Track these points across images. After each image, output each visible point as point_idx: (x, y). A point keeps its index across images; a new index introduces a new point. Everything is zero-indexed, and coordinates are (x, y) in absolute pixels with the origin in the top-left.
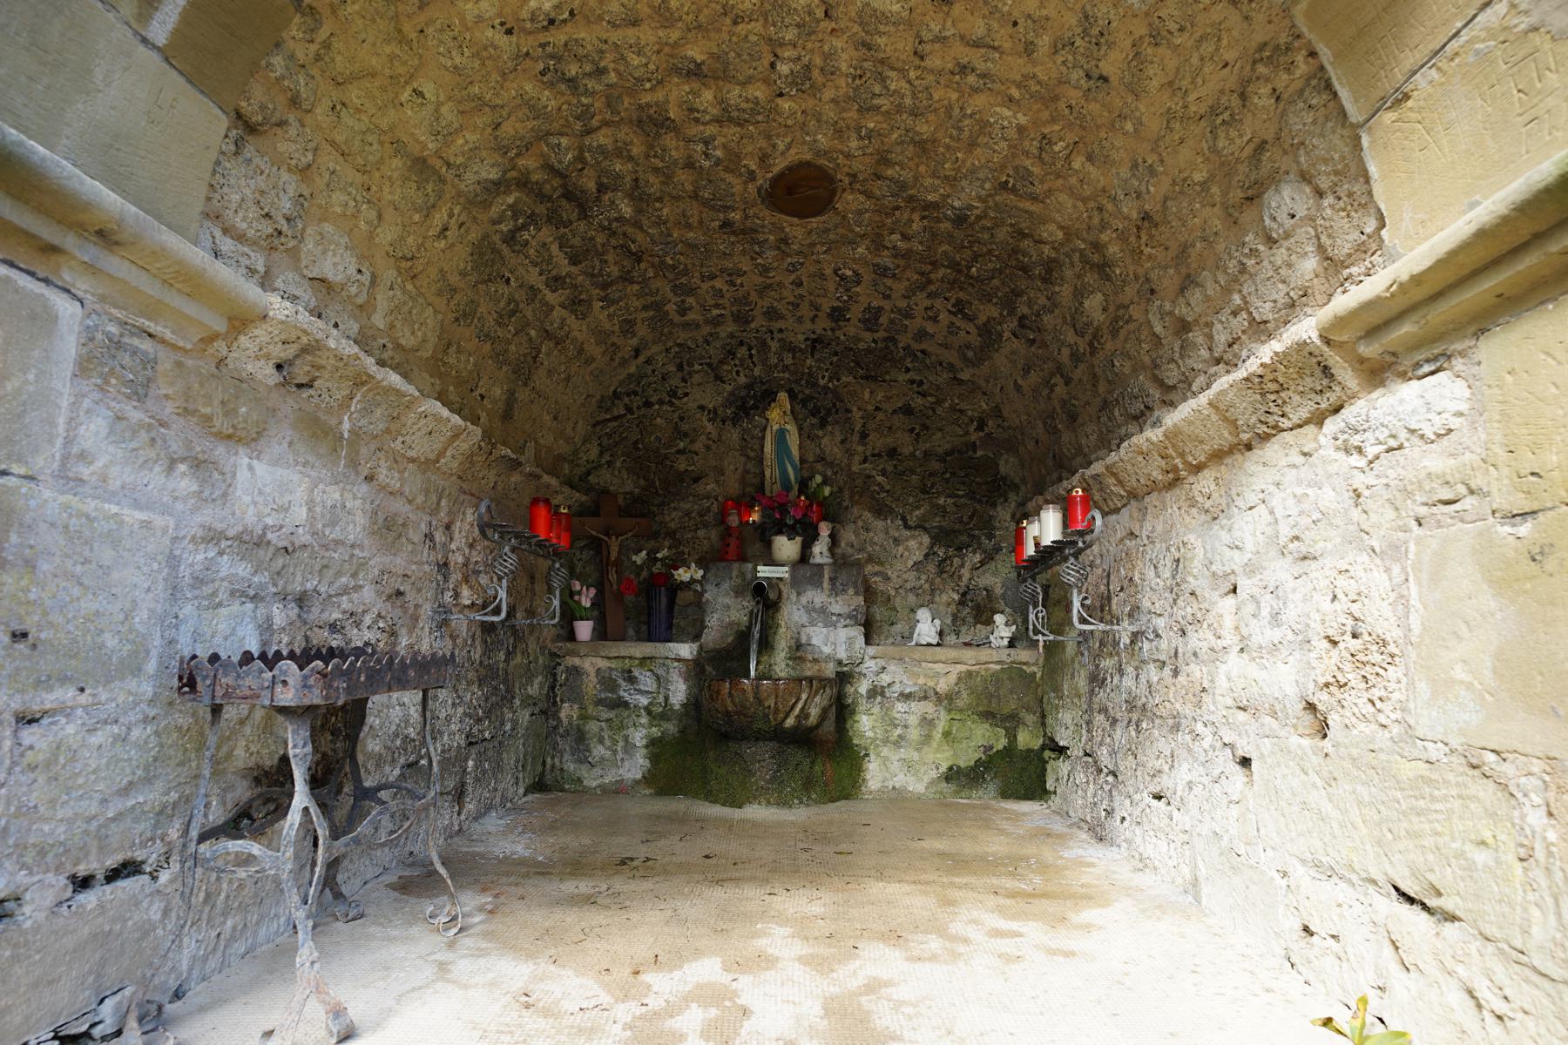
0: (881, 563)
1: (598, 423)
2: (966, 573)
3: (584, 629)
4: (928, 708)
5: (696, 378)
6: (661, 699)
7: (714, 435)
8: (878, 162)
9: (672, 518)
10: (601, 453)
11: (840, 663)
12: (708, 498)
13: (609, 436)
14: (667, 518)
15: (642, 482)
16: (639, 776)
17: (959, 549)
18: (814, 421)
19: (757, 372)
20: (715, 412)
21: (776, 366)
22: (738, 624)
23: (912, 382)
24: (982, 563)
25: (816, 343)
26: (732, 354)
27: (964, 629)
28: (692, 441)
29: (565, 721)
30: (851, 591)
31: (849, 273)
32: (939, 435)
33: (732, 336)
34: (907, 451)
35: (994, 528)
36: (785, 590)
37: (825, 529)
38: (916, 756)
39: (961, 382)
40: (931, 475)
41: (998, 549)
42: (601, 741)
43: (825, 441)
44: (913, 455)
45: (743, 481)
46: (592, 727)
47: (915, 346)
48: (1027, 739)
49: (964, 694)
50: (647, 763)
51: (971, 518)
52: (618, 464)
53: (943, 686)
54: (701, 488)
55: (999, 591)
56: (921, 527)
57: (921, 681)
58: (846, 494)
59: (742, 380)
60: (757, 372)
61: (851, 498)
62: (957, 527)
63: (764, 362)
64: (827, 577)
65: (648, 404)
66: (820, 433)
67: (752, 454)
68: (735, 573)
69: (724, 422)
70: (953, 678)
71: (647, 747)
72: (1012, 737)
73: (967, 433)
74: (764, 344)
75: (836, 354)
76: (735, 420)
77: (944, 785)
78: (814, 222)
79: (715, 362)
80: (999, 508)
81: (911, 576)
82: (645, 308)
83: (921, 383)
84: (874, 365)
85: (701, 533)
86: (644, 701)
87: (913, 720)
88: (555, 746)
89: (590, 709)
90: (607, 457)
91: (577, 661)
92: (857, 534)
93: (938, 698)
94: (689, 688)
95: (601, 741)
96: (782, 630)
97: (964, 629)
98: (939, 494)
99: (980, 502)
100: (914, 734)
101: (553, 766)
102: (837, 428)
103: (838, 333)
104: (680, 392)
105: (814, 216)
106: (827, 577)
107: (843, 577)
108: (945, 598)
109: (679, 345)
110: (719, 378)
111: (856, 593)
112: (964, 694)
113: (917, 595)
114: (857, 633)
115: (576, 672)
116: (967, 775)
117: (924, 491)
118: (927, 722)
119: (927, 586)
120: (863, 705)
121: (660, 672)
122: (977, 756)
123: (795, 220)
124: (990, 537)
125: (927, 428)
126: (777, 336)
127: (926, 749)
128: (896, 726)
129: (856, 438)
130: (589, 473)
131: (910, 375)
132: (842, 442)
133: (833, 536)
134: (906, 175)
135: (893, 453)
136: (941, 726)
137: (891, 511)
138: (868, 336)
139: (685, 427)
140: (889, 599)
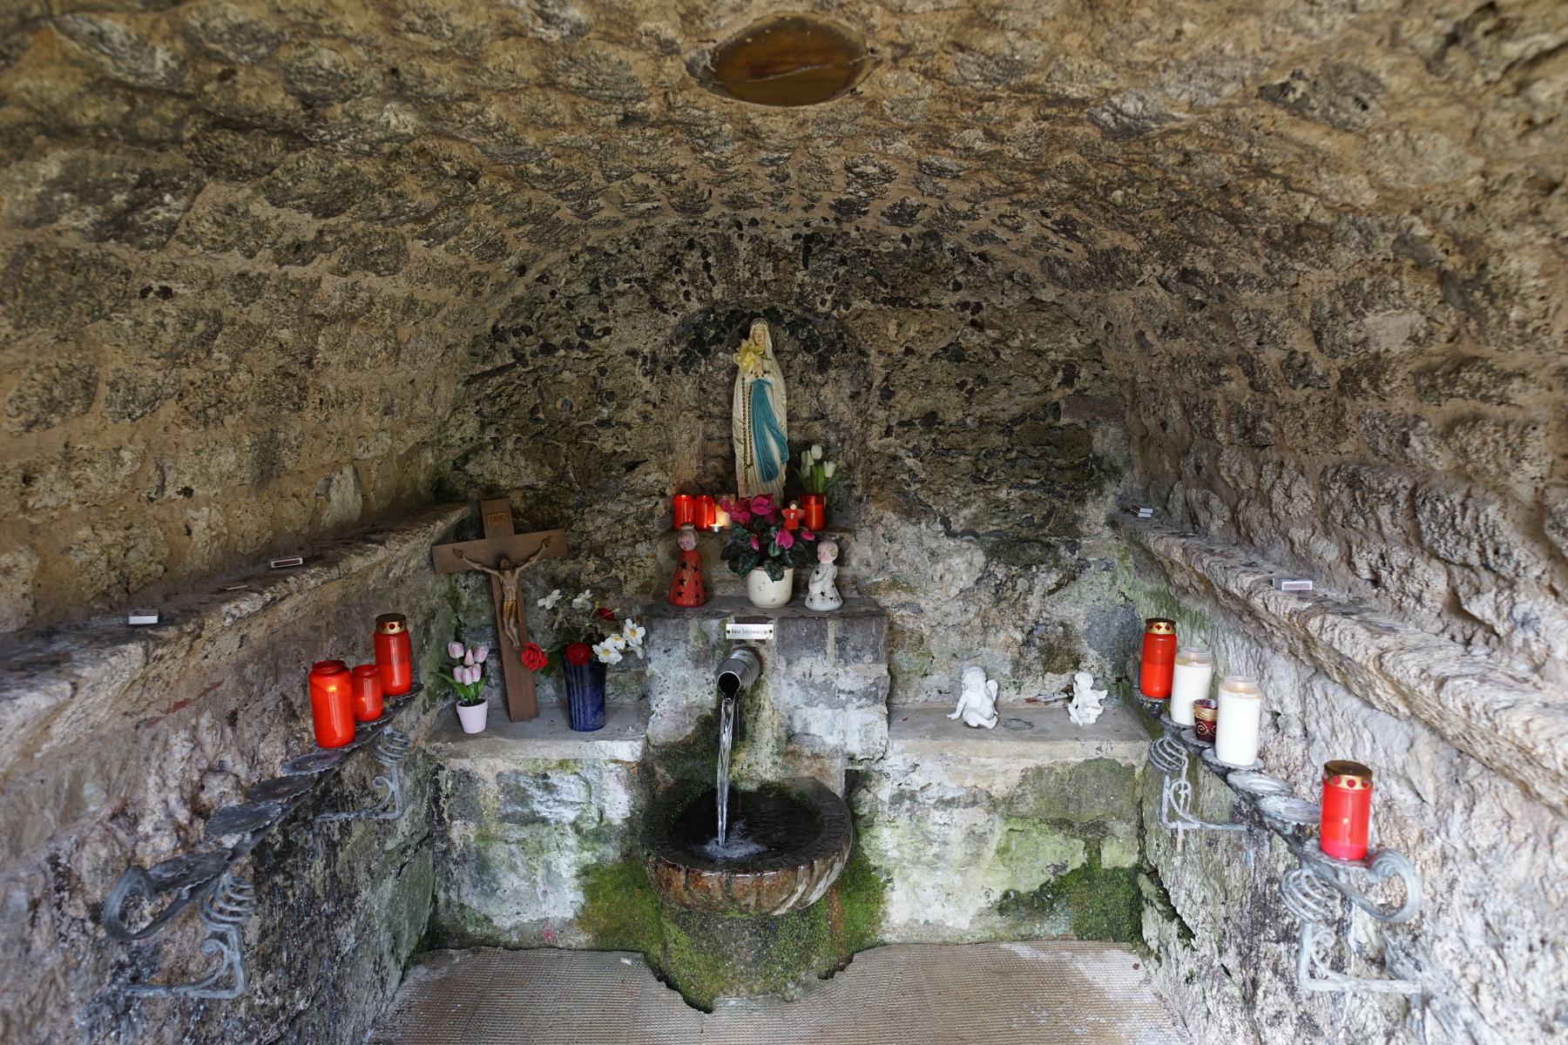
0: (910, 590)
1: (473, 379)
2: (1034, 601)
3: (474, 718)
4: (977, 816)
5: (622, 304)
6: (594, 813)
7: (655, 396)
8: (968, 22)
9: (597, 525)
10: (483, 427)
11: (852, 758)
12: (650, 496)
13: (492, 399)
14: (590, 527)
15: (548, 471)
16: (570, 915)
17: (1028, 567)
18: (809, 358)
19: (717, 293)
20: (655, 360)
21: (747, 284)
22: (701, 707)
23: (964, 305)
24: (1059, 586)
25: (810, 243)
26: (676, 261)
27: (1028, 681)
28: (621, 407)
29: (458, 842)
30: (868, 658)
31: (871, 170)
32: (1003, 393)
33: (674, 232)
34: (952, 418)
35: (1079, 535)
36: (768, 656)
37: (827, 553)
38: (957, 880)
39: (1040, 305)
40: (989, 455)
41: (1082, 566)
42: (513, 868)
43: (827, 392)
44: (962, 423)
45: (704, 456)
46: (498, 852)
47: (971, 248)
48: (1117, 854)
49: (1030, 798)
50: (580, 897)
51: (1047, 518)
52: (510, 445)
53: (999, 789)
54: (639, 479)
55: (1081, 626)
56: (970, 532)
57: (969, 782)
58: (859, 478)
59: (694, 305)
60: (717, 293)
61: (867, 487)
62: (1024, 533)
63: (728, 277)
64: (831, 637)
65: (548, 349)
66: (819, 378)
67: (716, 410)
68: (692, 634)
69: (668, 369)
70: (1015, 778)
71: (578, 877)
72: (1094, 852)
73: (1047, 389)
74: (727, 245)
75: (843, 261)
76: (687, 363)
77: (996, 918)
78: (811, 111)
79: (649, 276)
80: (1090, 504)
81: (955, 607)
83: (978, 307)
84: (903, 278)
85: (642, 548)
86: (570, 815)
87: (956, 835)
88: (448, 876)
89: (493, 827)
90: (490, 434)
91: (466, 764)
92: (875, 547)
93: (994, 804)
94: (633, 798)
95: (513, 868)
96: (766, 714)
97: (1028, 681)
98: (999, 483)
99: (1061, 496)
100: (957, 852)
101: (448, 902)
102: (845, 375)
103: (846, 227)
104: (597, 327)
105: (813, 102)
106: (831, 637)
107: (856, 638)
108: (1002, 636)
109: (591, 250)
110: (656, 304)
111: (877, 661)
112: (1030, 798)
113: (964, 634)
114: (875, 715)
115: (466, 778)
116: (1029, 904)
117: (977, 480)
118: (976, 837)
119: (977, 621)
120: (886, 813)
121: (590, 775)
122: (1043, 879)
123: (777, 109)
124: (1073, 547)
125: (985, 381)
126: (749, 231)
127: (972, 870)
128: (931, 843)
129: (875, 397)
130: (466, 459)
131: (962, 295)
132: (853, 396)
133: (840, 561)
134: (1027, 50)
135: (930, 419)
136: (994, 842)
137: (927, 510)
138: (896, 233)
139: (608, 384)
140: (921, 640)
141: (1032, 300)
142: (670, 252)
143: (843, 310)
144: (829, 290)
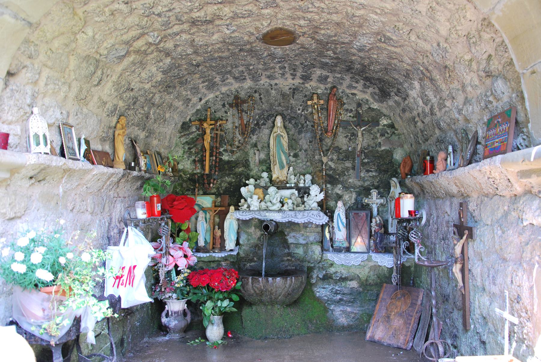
33: (250, 88)
47: (348, 91)
82: (203, 82)
103: (306, 85)
138: (322, 86)
141: (370, 108)
142: (249, 94)
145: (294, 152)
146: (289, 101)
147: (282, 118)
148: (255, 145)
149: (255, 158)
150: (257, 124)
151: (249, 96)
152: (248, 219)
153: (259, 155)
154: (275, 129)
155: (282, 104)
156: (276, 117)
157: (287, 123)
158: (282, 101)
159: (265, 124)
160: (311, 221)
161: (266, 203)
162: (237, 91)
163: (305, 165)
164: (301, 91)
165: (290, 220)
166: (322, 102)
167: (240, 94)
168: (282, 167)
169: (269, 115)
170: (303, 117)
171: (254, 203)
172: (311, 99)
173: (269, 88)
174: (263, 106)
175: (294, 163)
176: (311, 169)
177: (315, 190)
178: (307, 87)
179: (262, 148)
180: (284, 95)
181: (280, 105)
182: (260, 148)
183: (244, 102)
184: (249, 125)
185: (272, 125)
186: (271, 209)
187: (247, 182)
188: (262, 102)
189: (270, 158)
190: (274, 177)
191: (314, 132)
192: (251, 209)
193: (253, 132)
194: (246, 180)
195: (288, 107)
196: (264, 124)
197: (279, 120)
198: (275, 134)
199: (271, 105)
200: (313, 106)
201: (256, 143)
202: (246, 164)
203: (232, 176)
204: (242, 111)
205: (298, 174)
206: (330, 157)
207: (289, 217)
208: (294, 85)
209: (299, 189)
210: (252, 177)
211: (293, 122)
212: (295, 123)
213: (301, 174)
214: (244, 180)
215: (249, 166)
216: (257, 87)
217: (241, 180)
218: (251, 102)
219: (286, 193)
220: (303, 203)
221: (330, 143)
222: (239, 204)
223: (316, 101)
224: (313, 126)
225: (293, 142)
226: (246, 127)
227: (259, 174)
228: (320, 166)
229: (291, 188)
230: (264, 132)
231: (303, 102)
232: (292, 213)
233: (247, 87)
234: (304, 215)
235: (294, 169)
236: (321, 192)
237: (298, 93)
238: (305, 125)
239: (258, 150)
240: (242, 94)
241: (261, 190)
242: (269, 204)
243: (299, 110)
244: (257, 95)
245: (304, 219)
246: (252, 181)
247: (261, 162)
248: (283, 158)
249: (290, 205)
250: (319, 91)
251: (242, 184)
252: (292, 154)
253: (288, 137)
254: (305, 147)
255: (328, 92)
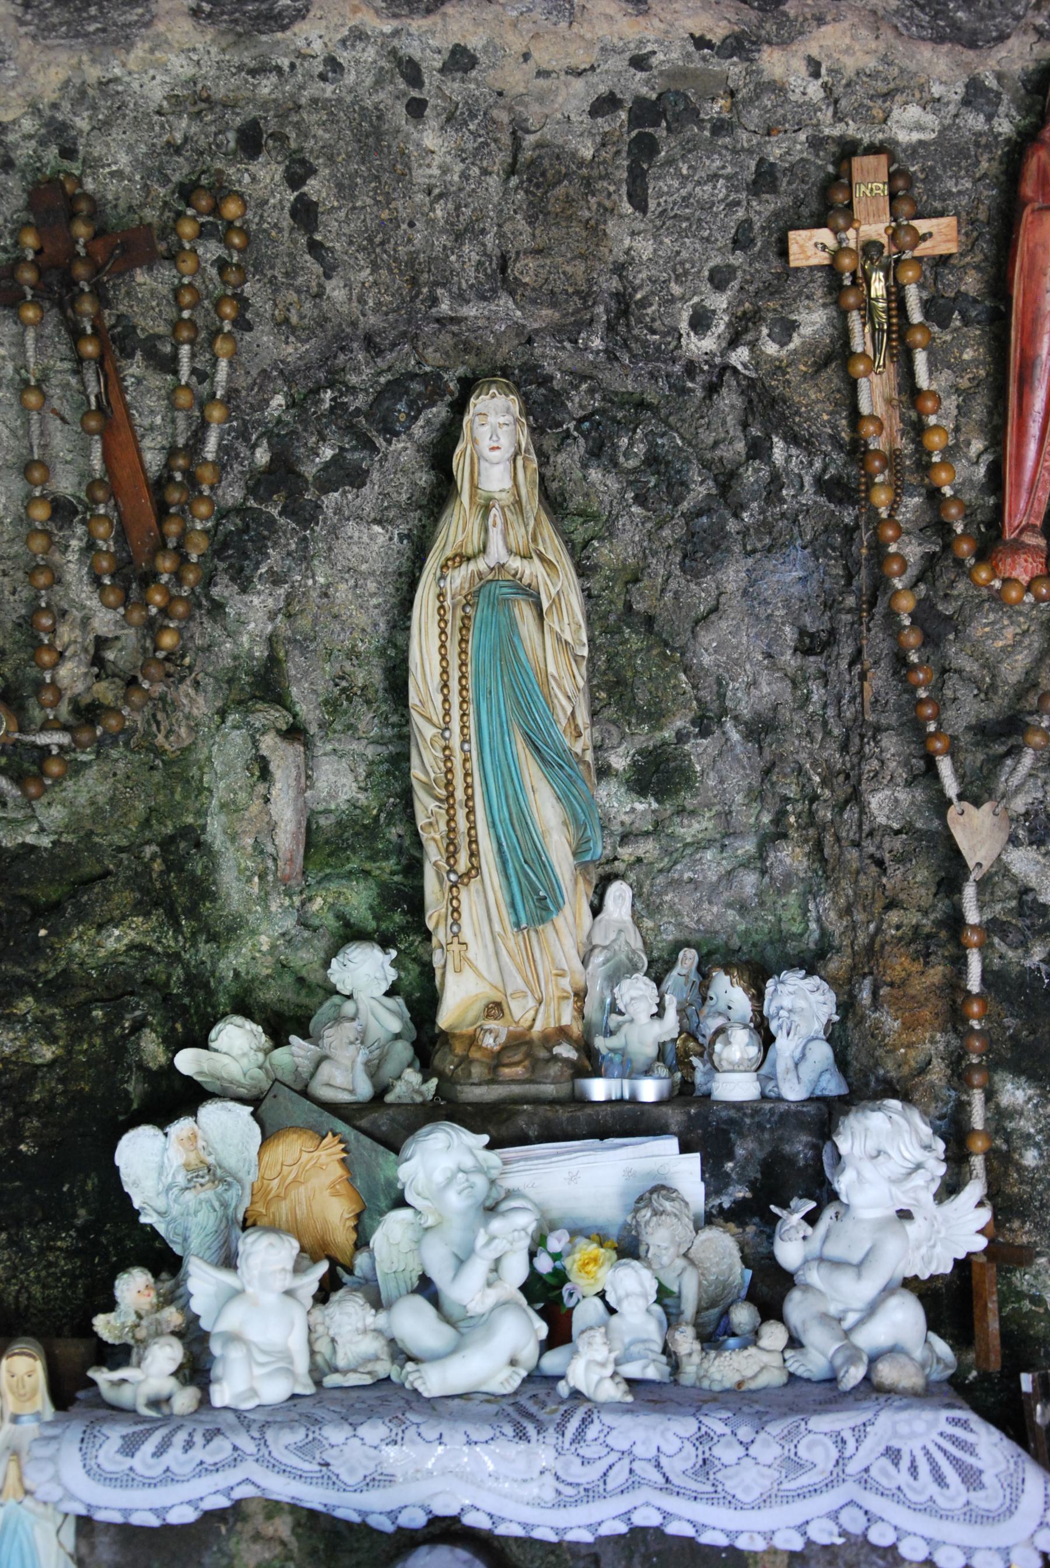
33: (195, 100)
103: (773, 62)
138: (941, 68)
142: (180, 170)
143: (771, 348)
144: (719, 279)
145: (644, 737)
146: (595, 231)
147: (528, 410)
148: (266, 684)
149: (265, 807)
150: (281, 476)
151: (187, 192)
152: (183, 1516)
153: (307, 778)
154: (457, 528)
155: (526, 270)
156: (459, 407)
157: (568, 460)
158: (523, 233)
159: (357, 478)
160: (881, 1536)
161: (377, 1303)
162: (57, 132)
163: (759, 861)
164: (720, 127)
165: (641, 1519)
166: (940, 235)
167: (92, 164)
168: (535, 904)
169: (397, 387)
170: (729, 400)
171: (262, 1318)
172: (829, 205)
173: (390, 102)
174: (336, 291)
175: (647, 848)
176: (826, 908)
177: (886, 1154)
178: (778, 88)
179: (331, 705)
180: (539, 174)
181: (501, 274)
182: (308, 711)
183: (133, 245)
184: (192, 480)
185: (424, 478)
186: (433, 1381)
187: (187, 1061)
188: (315, 248)
189: (407, 797)
190: (458, 1002)
191: (863, 571)
192: (221, 1395)
193: (238, 549)
194: (174, 1045)
195: (587, 296)
196: (346, 475)
197: (494, 425)
198: (459, 578)
199: (419, 277)
200: (836, 283)
201: (273, 661)
202: (177, 881)
203: (26, 1005)
204: (120, 341)
205: (689, 958)
206: (1019, 804)
207: (634, 1482)
208: (639, 62)
209: (707, 1131)
210: (243, 1007)
211: (630, 448)
212: (653, 460)
213: (715, 957)
214: (151, 1047)
215: (203, 891)
216: (266, 86)
217: (120, 1050)
218: (211, 251)
219: (588, 1178)
220: (771, 1289)
221: (1022, 660)
222: (104, 1325)
223: (874, 228)
224: (835, 489)
225: (635, 641)
226: (162, 510)
227: (305, 958)
228: (923, 895)
229: (627, 1122)
230: (347, 553)
231: (741, 241)
232: (667, 1436)
233: (157, 93)
234: (794, 1464)
235: (645, 906)
236: (950, 1189)
237: (690, 147)
238: (752, 475)
239: (295, 733)
240: (116, 169)
241: (330, 1152)
242: (415, 1324)
243: (701, 322)
244: (265, 175)
245: (800, 1511)
246: (235, 1047)
247: (327, 844)
248: (547, 811)
249: (640, 1320)
250: (909, 124)
251: (134, 1087)
252: (619, 761)
253: (588, 595)
254: (757, 690)
255: (1004, 127)
